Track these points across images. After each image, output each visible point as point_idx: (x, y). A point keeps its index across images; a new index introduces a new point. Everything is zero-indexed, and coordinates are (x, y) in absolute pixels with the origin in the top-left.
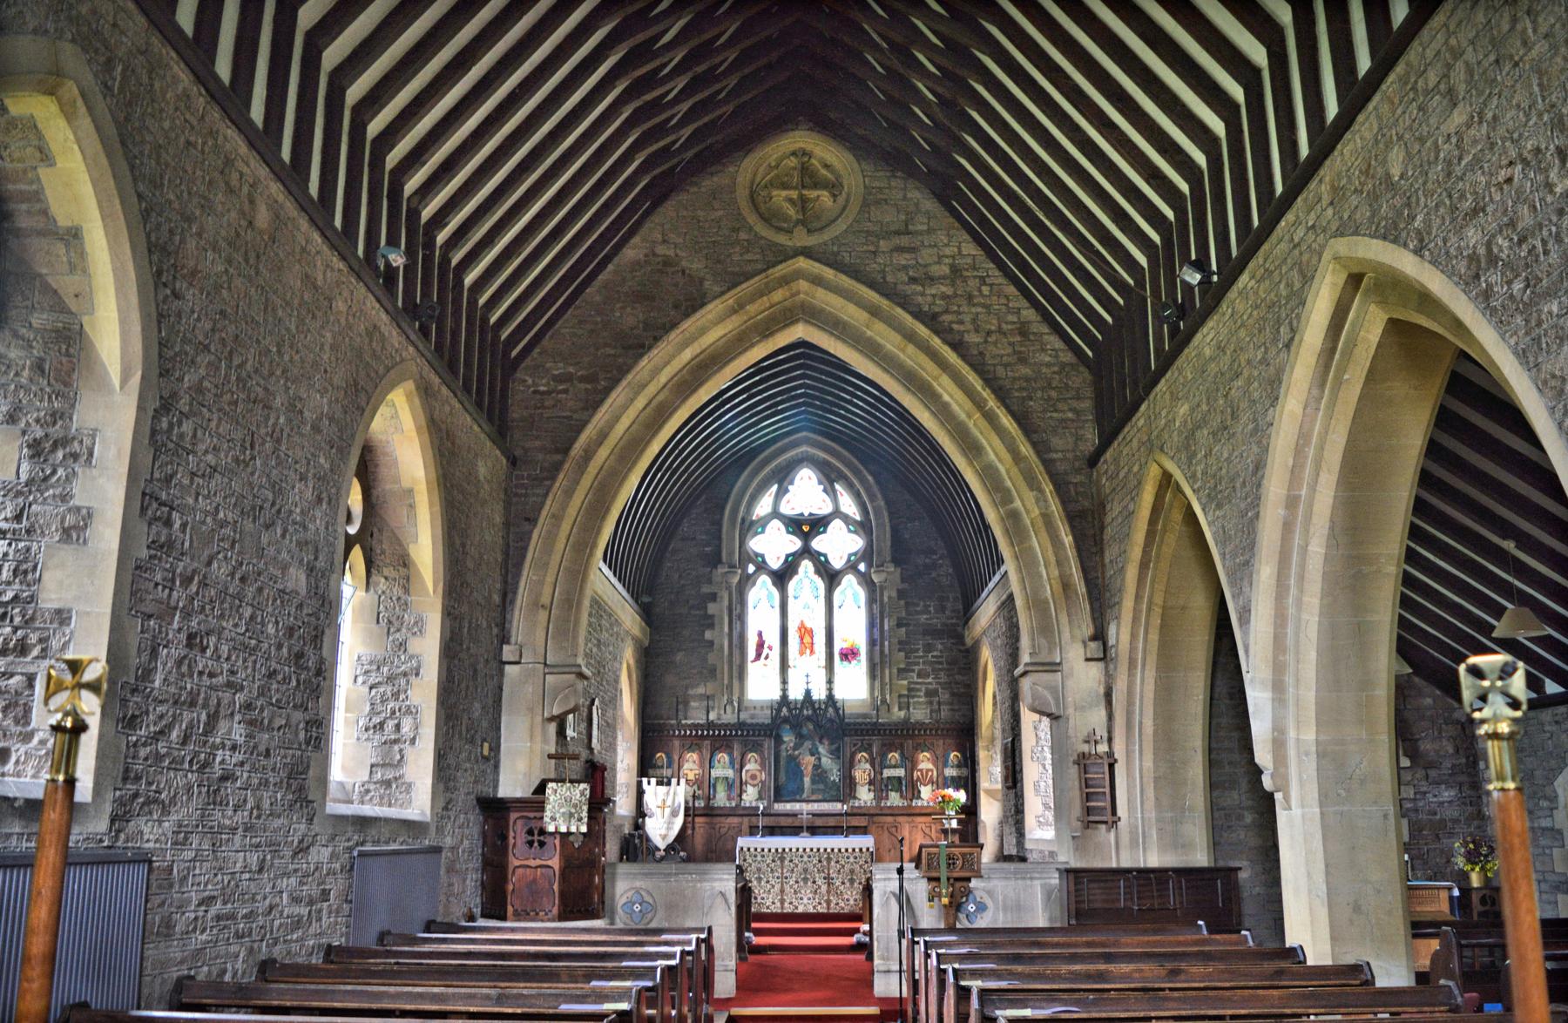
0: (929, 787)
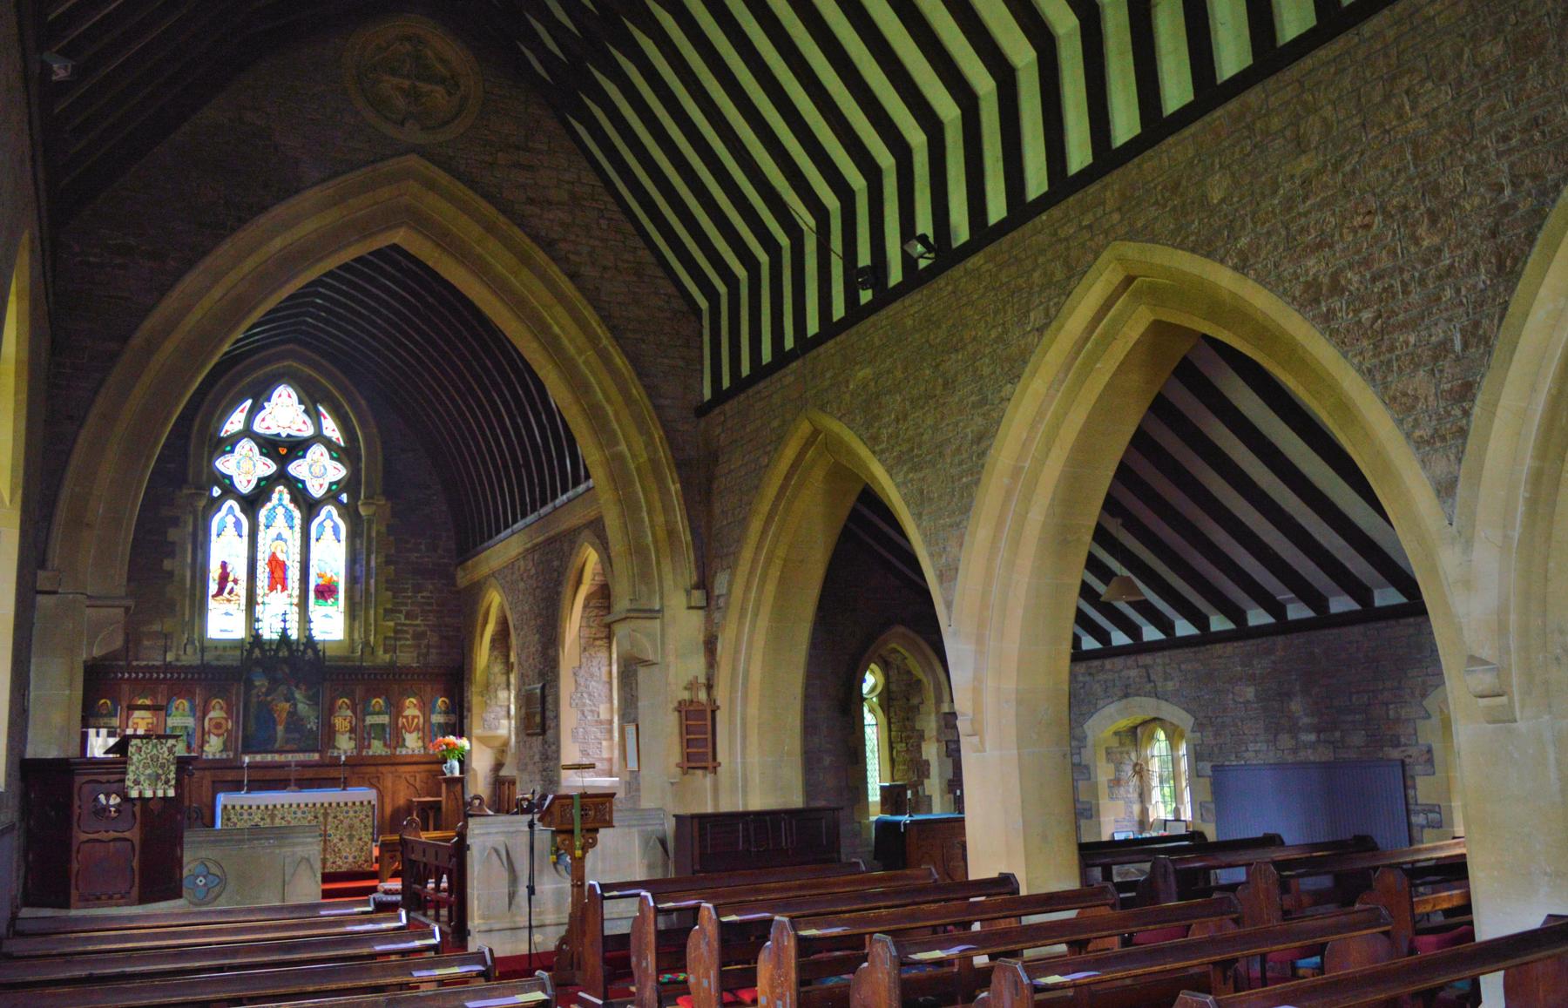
0: (415, 735)
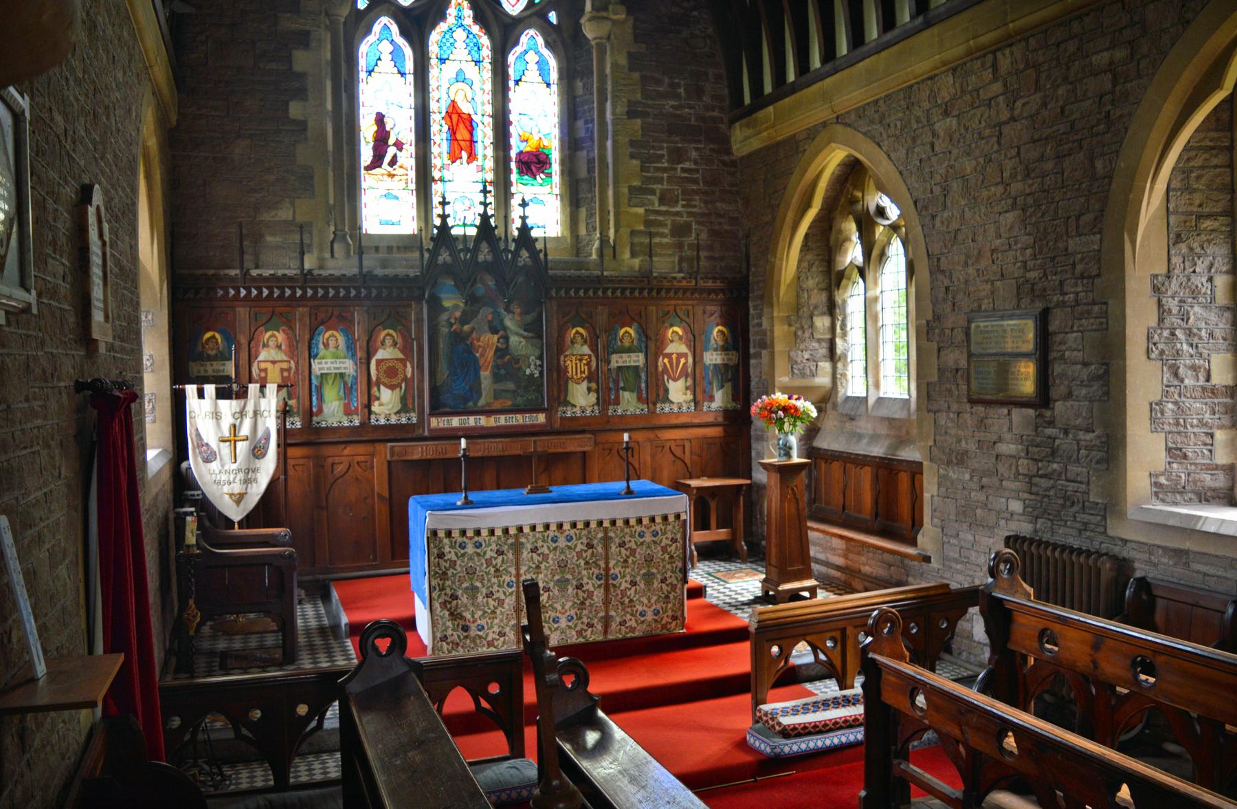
0: (681, 384)
